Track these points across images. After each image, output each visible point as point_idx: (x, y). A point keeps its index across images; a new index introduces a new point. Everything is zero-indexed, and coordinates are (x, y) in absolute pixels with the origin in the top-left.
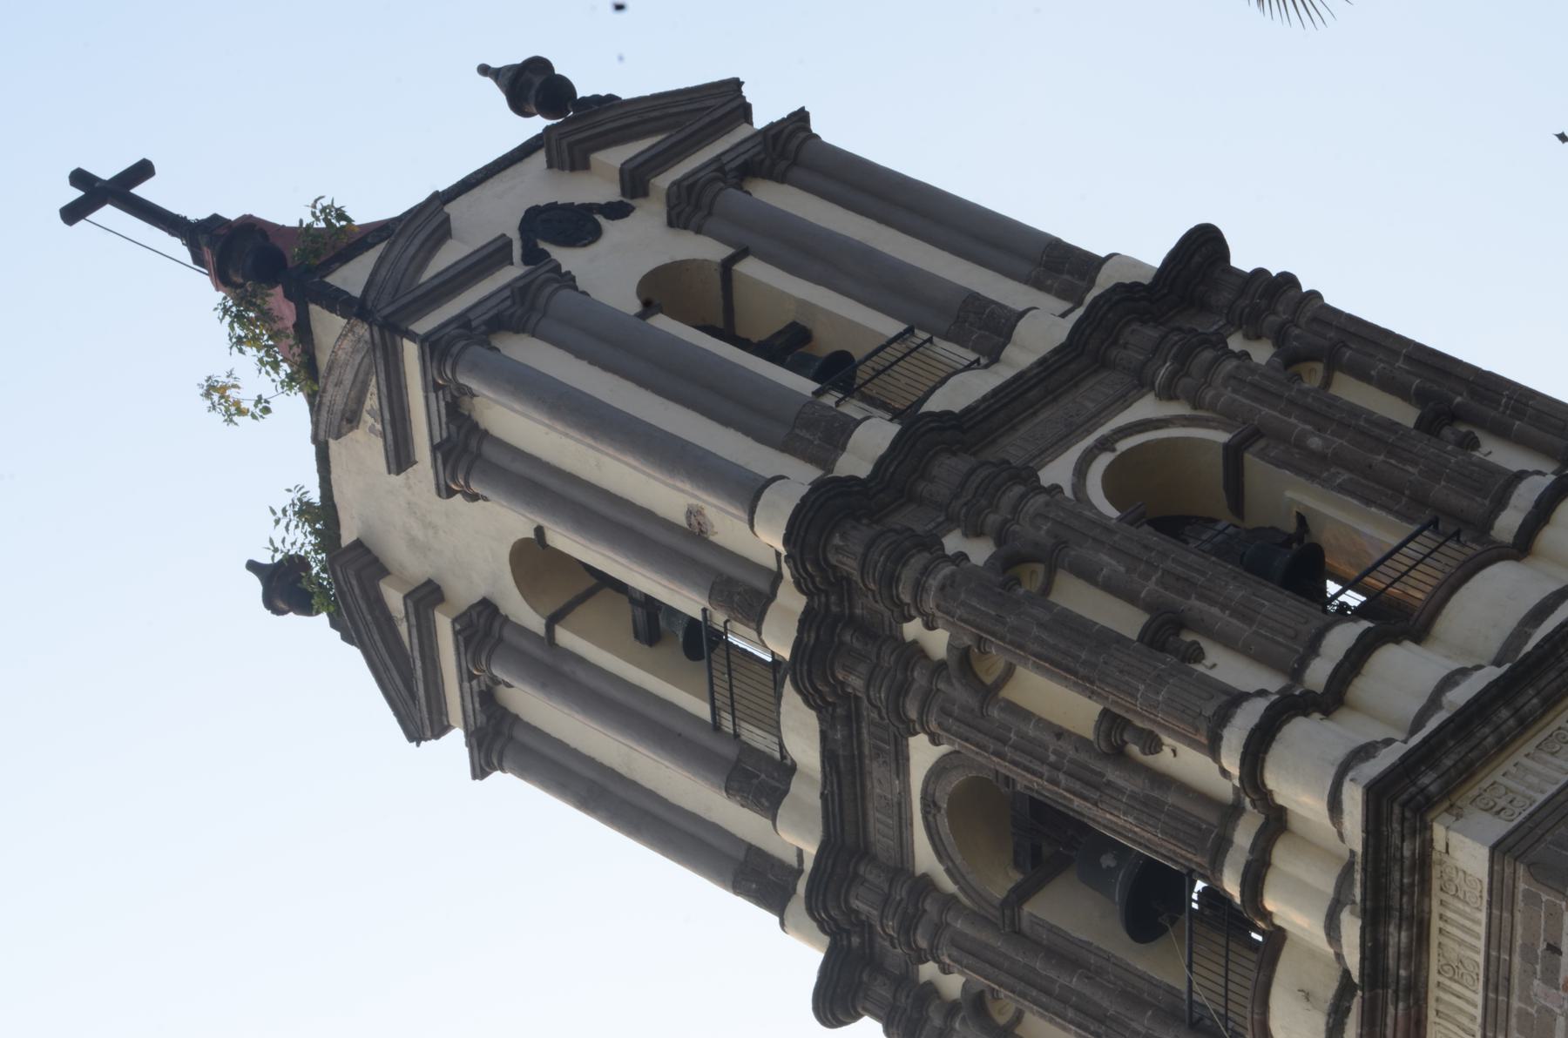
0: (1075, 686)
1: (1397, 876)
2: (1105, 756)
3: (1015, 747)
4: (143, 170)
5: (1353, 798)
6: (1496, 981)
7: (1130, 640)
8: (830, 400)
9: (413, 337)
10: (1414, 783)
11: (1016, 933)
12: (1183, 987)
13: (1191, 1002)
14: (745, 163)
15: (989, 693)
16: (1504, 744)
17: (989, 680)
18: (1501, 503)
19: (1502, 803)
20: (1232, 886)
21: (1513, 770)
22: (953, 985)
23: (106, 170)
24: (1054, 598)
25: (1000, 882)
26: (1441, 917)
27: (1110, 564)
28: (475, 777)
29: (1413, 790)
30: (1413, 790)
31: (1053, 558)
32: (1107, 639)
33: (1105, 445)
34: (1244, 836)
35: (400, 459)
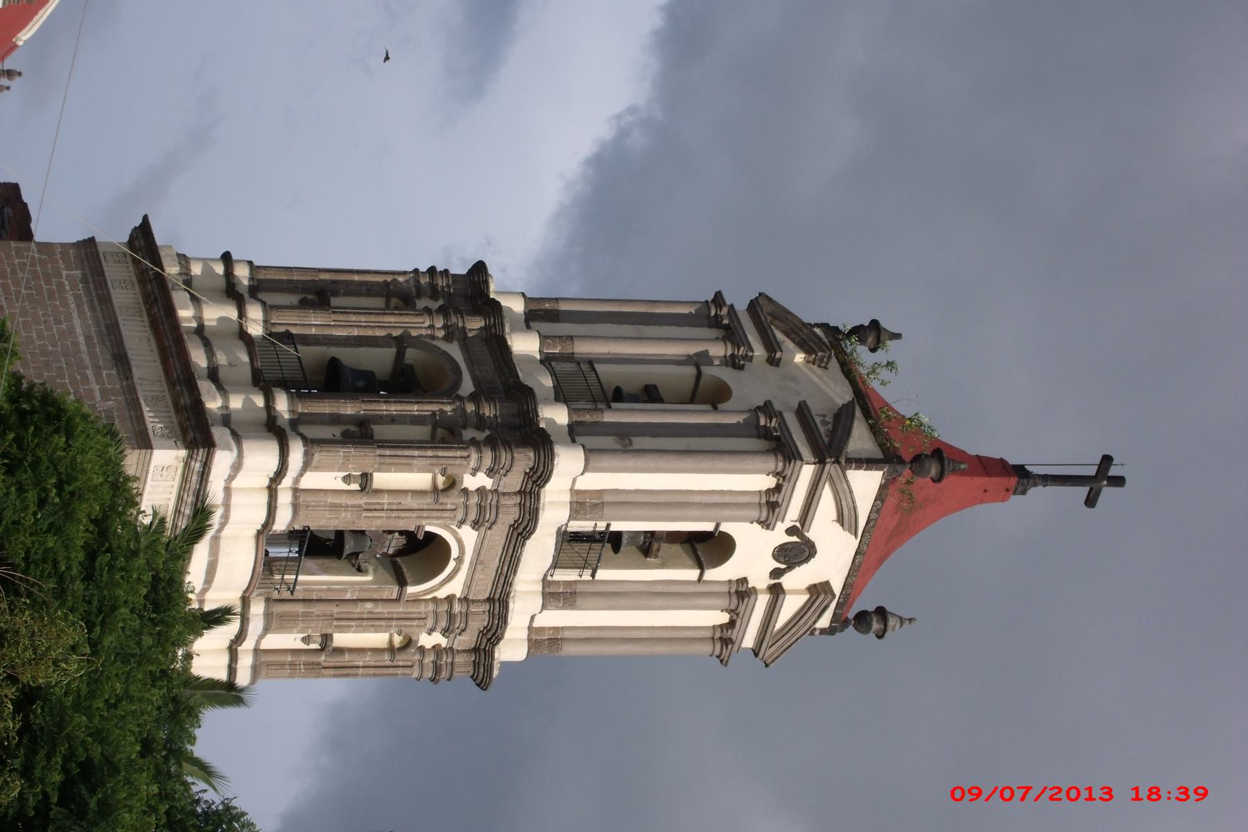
1: (193, 423)
7: (376, 472)
10: (201, 461)
12: (299, 347)
13: (294, 343)
14: (734, 626)
18: (268, 616)
19: (165, 473)
21: (170, 490)
23: (1108, 494)
26: (171, 417)
28: (720, 292)
29: (200, 458)
30: (200, 458)
33: (460, 560)
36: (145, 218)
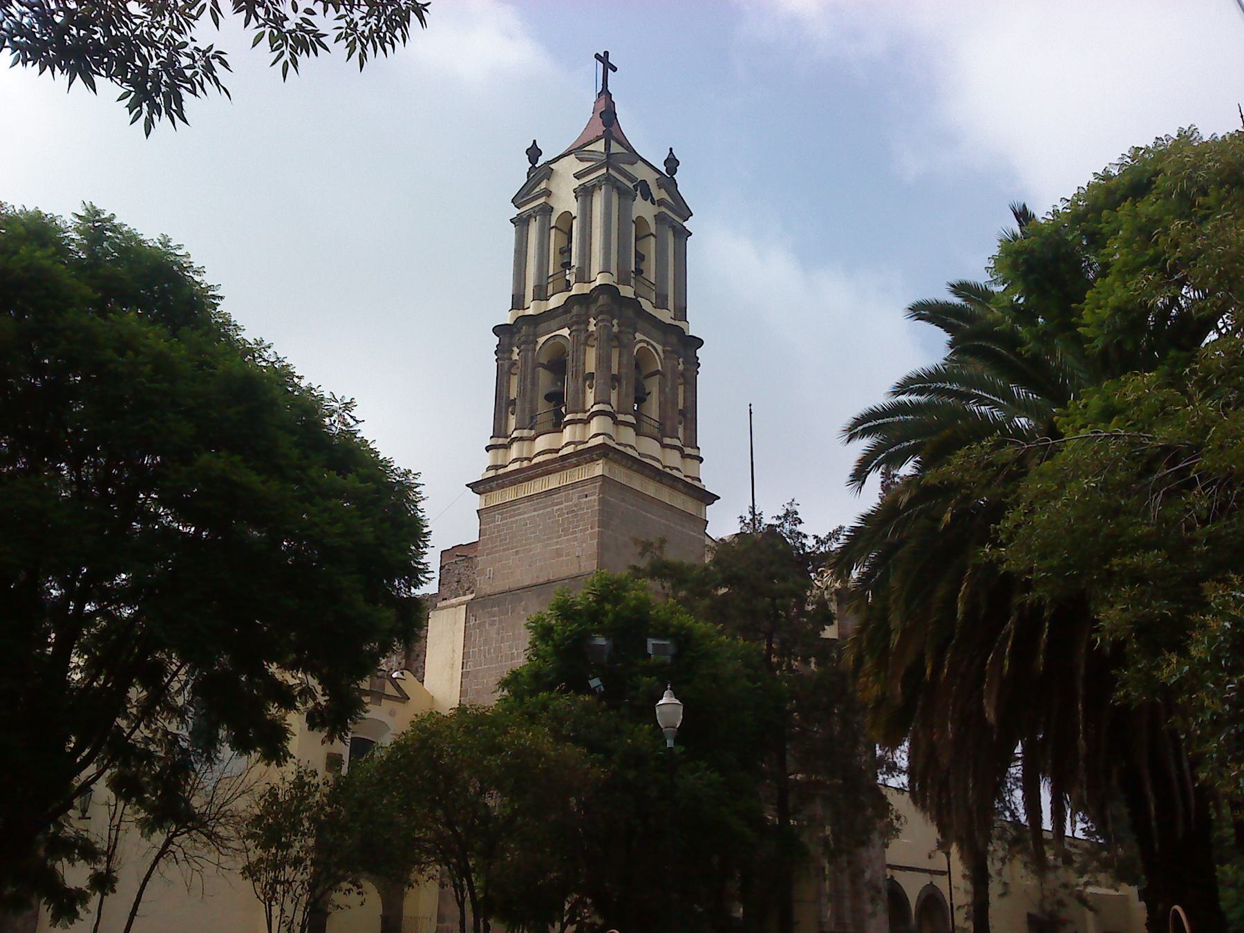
0: (596, 364)
2: (584, 377)
3: (577, 355)
4: (615, 69)
5: (599, 440)
6: (574, 485)
8: (633, 275)
9: (607, 170)
11: (534, 369)
15: (586, 344)
16: (624, 466)
17: (589, 343)
20: (568, 418)
22: (515, 357)
24: (613, 349)
25: (544, 360)
27: (625, 359)
31: (621, 346)
32: (610, 368)
33: (648, 343)
34: (579, 416)
35: (578, 176)
36: (467, 485)
